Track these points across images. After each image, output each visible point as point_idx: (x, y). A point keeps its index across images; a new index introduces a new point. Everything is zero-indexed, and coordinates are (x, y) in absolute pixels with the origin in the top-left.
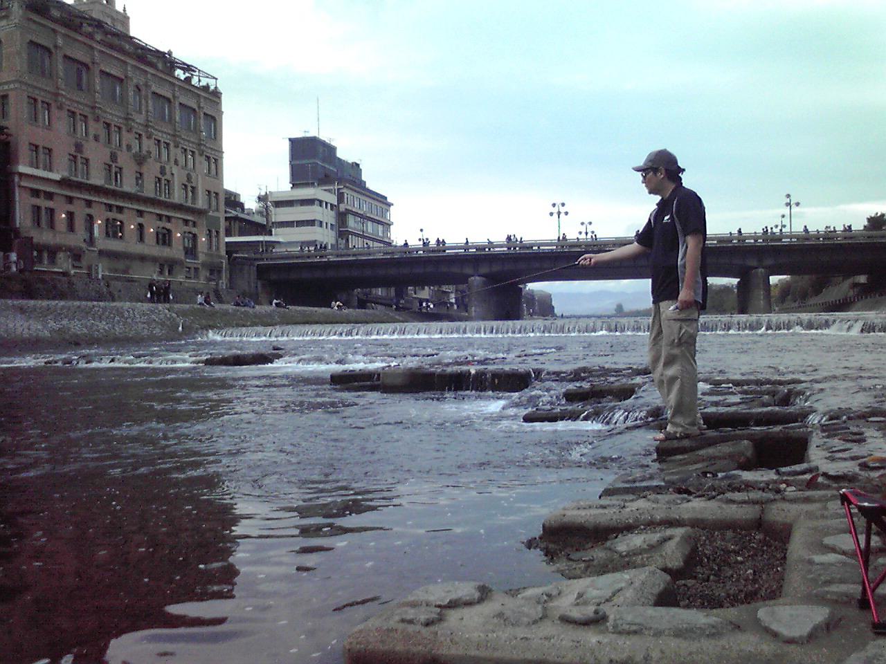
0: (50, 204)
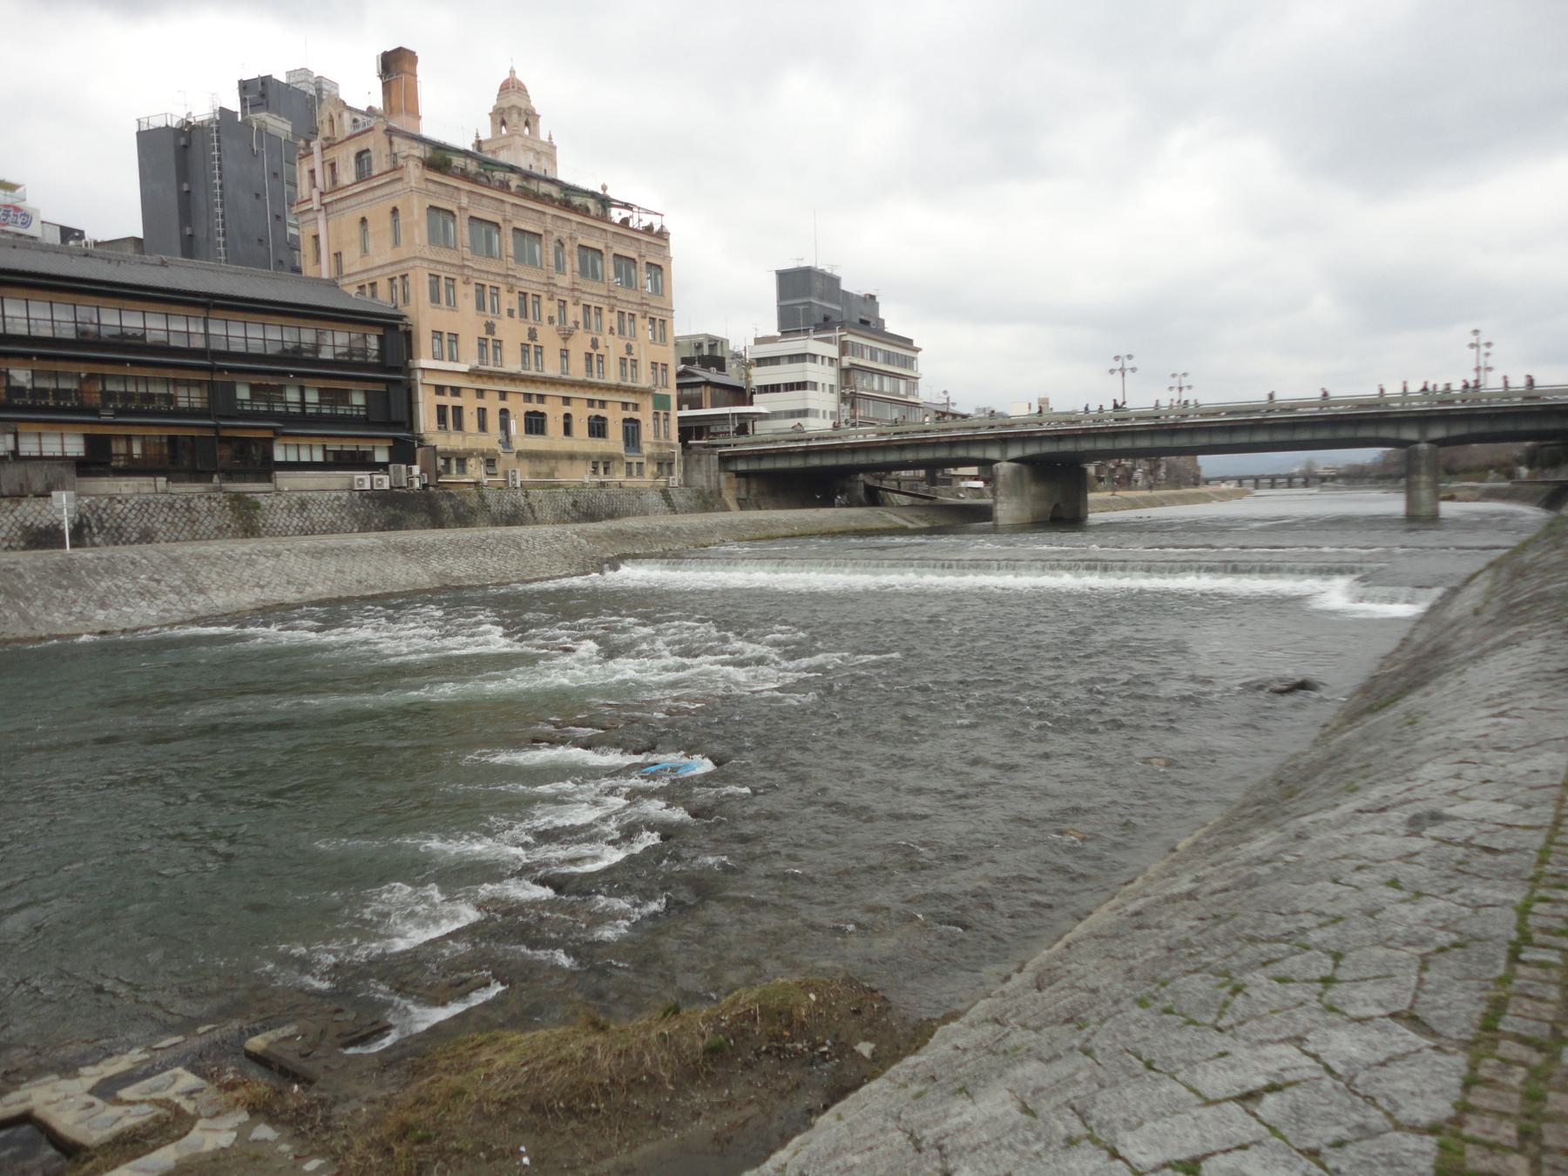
0: (457, 401)
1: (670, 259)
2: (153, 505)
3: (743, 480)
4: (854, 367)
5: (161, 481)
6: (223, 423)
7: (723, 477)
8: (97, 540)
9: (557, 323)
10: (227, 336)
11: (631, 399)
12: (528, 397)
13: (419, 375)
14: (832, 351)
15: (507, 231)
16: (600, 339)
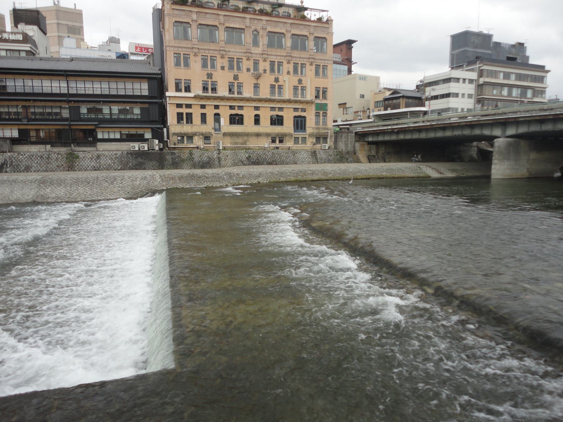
0: (189, 111)
1: (332, 34)
2: (34, 156)
3: (373, 147)
4: (486, 84)
5: (48, 147)
6: (71, 123)
7: (357, 145)
8: (8, 169)
9: (252, 71)
10: (15, 86)
11: (300, 106)
12: (232, 107)
13: (168, 99)
14: (474, 75)
15: (222, 28)
16: (280, 78)
